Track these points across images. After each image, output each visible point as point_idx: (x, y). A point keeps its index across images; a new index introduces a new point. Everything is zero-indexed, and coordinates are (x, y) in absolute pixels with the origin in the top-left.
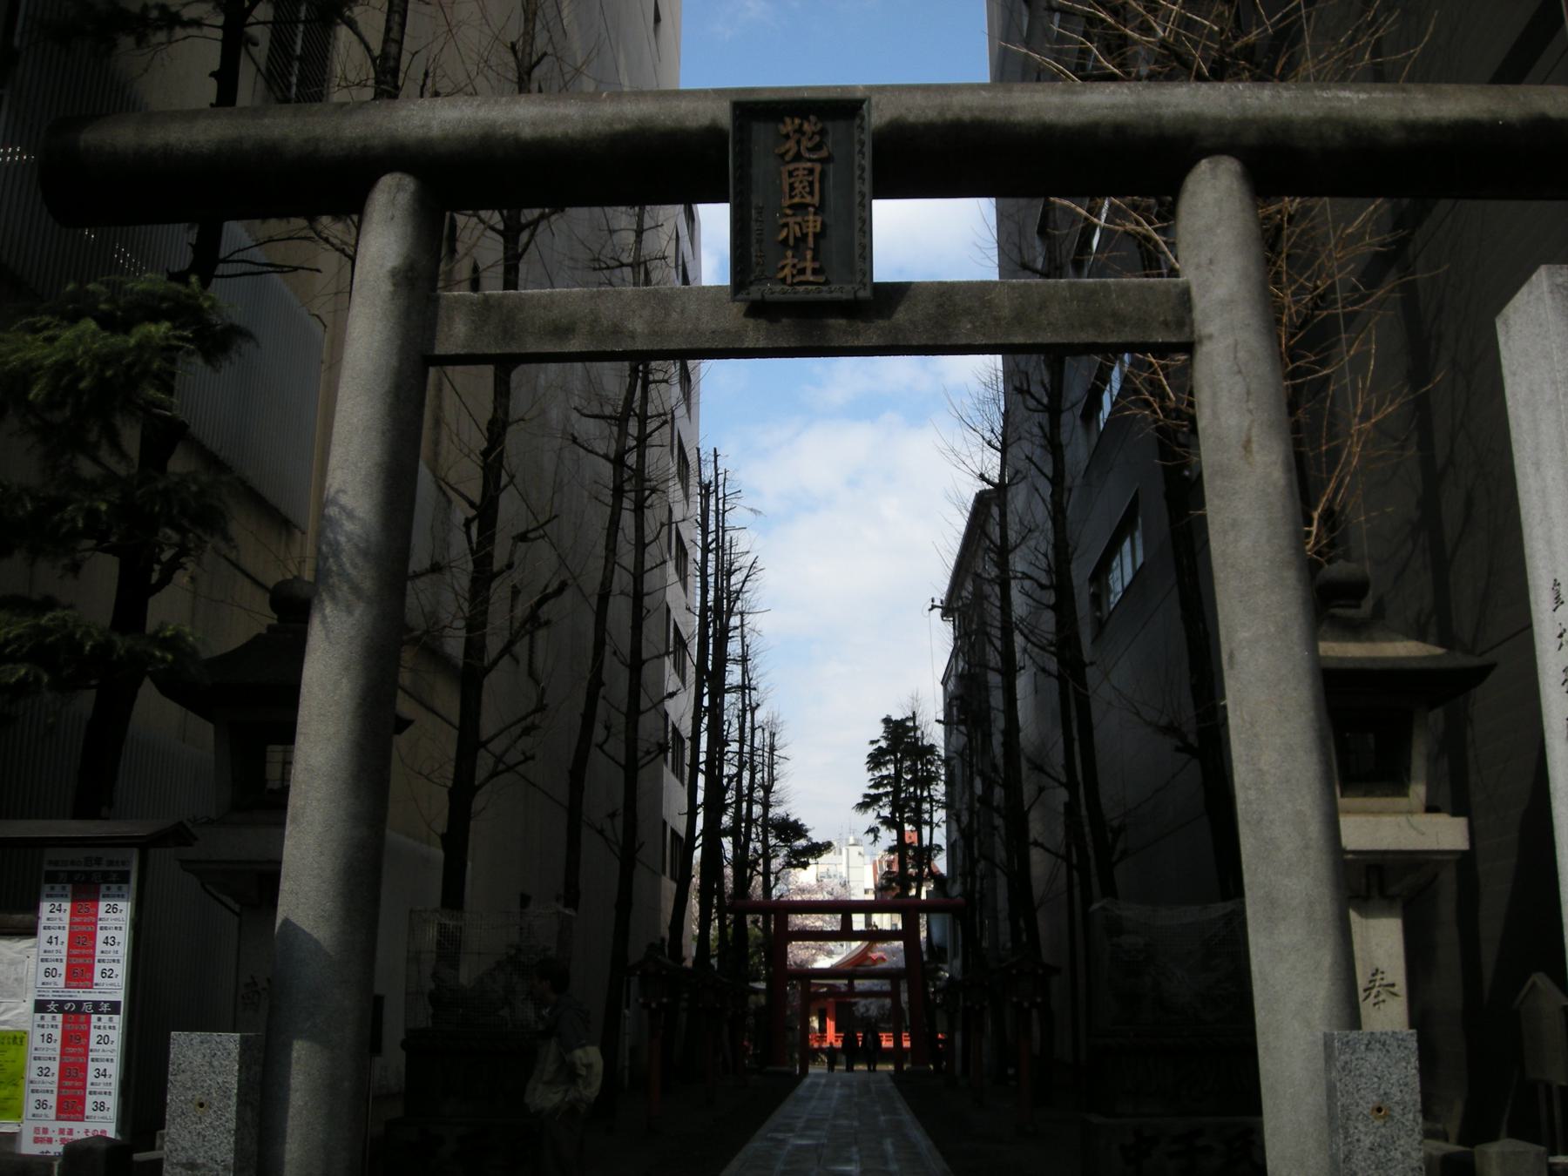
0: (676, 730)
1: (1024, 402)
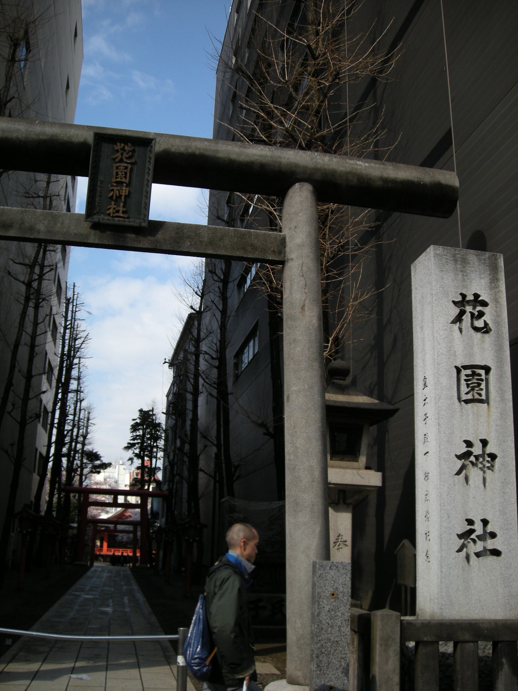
0: (45, 408)
1: (213, 277)
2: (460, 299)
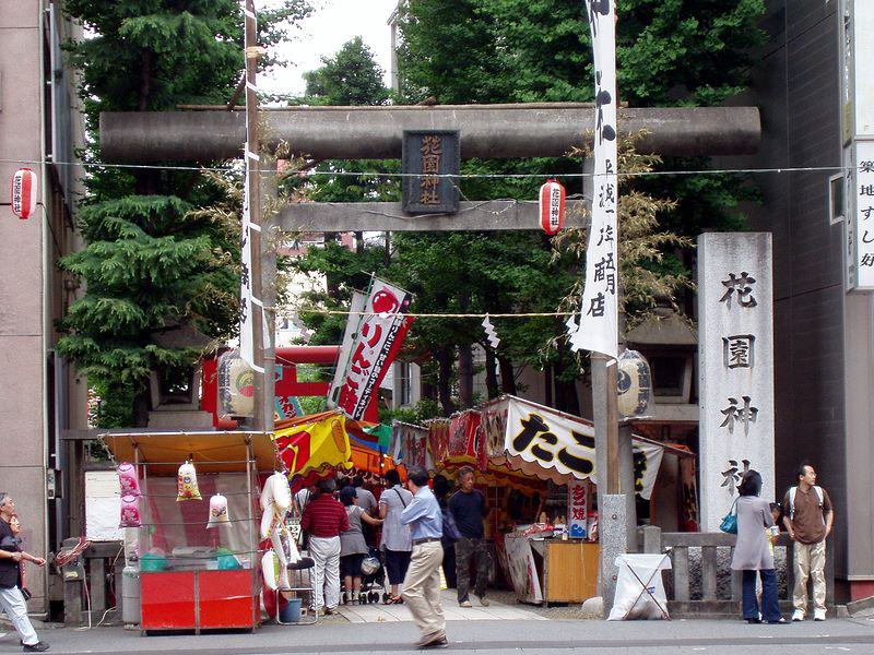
2: (729, 278)
